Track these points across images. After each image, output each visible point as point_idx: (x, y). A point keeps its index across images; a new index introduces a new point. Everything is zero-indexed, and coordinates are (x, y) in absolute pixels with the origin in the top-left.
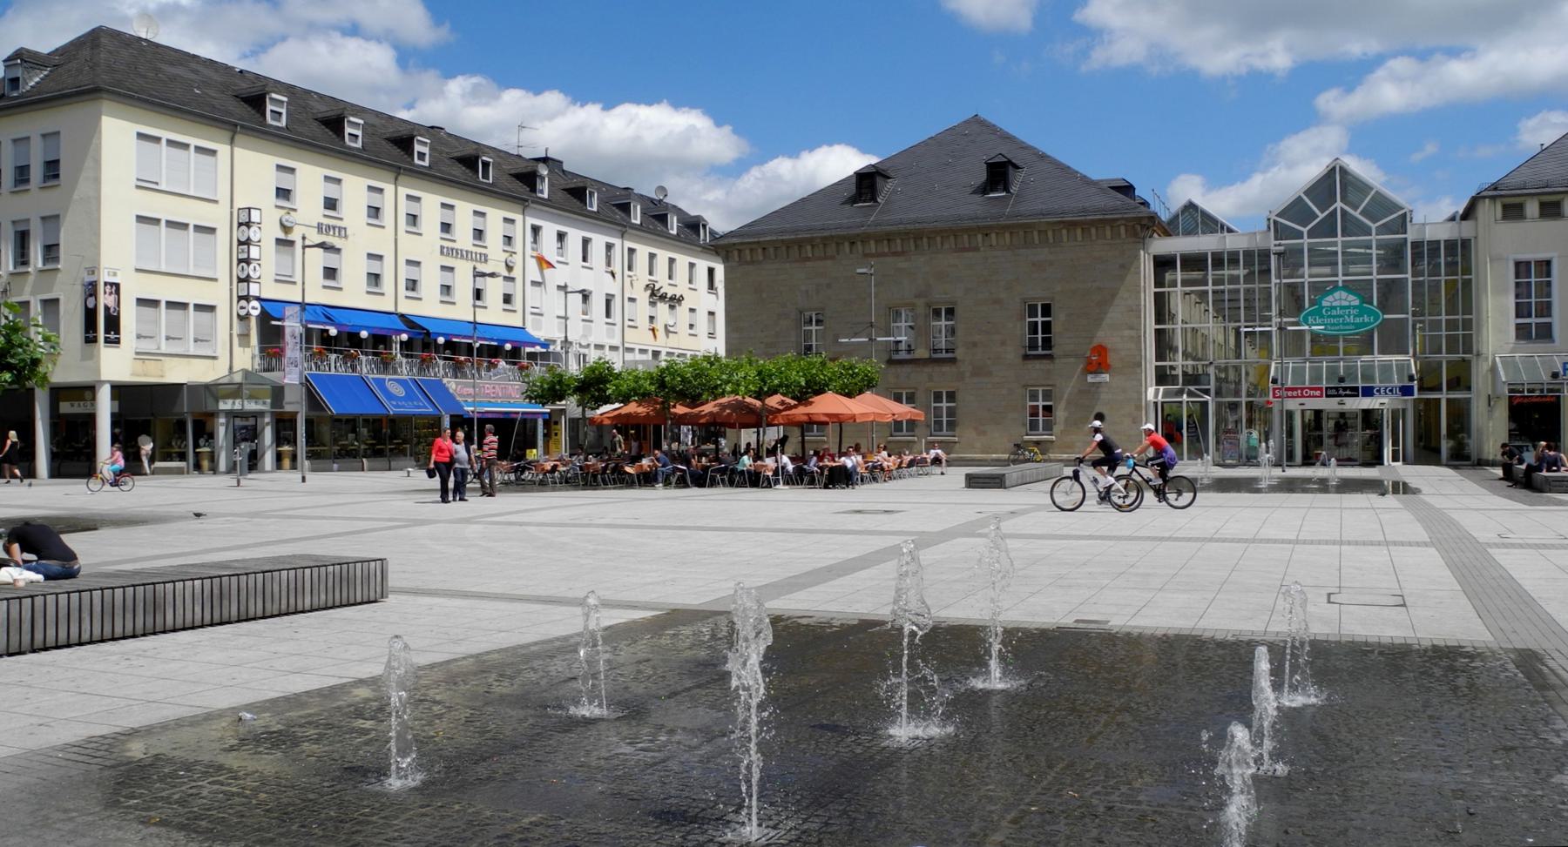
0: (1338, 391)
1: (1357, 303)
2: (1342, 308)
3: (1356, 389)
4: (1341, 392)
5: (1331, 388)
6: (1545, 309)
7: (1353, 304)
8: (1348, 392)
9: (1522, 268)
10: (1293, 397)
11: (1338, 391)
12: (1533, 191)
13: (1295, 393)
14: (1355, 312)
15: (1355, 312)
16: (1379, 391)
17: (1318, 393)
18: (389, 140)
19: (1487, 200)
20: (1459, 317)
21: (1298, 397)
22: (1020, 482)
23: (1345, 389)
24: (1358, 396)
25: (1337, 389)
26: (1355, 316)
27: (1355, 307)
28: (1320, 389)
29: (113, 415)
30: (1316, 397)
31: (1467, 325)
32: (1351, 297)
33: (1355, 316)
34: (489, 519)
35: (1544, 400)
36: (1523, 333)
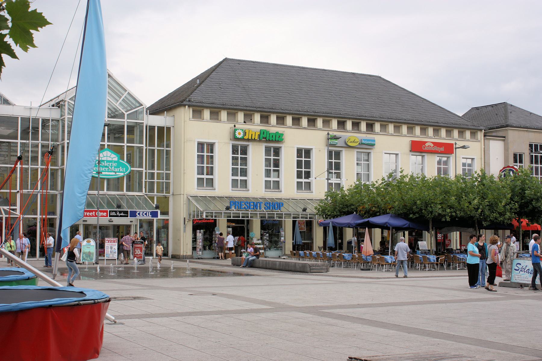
0: (116, 213)
1: (116, 159)
2: (108, 161)
3: (126, 212)
4: (118, 214)
5: (113, 211)
6: (211, 171)
7: (114, 159)
8: (122, 214)
9: (201, 146)
10: (90, 216)
11: (116, 213)
12: (207, 105)
13: (91, 214)
14: (115, 164)
15: (115, 164)
16: (139, 214)
17: (105, 214)
18: (36, 47)
19: (170, 104)
20: (30, 166)
21: (93, 216)
22: (264, 266)
23: (120, 212)
24: (127, 216)
25: (116, 212)
26: (115, 167)
27: (115, 162)
28: (106, 212)
29: (163, 215)
30: (104, 216)
31: (168, 176)
32: (113, 156)
33: (115, 167)
34: (328, 282)
35: (208, 221)
36: (200, 181)
